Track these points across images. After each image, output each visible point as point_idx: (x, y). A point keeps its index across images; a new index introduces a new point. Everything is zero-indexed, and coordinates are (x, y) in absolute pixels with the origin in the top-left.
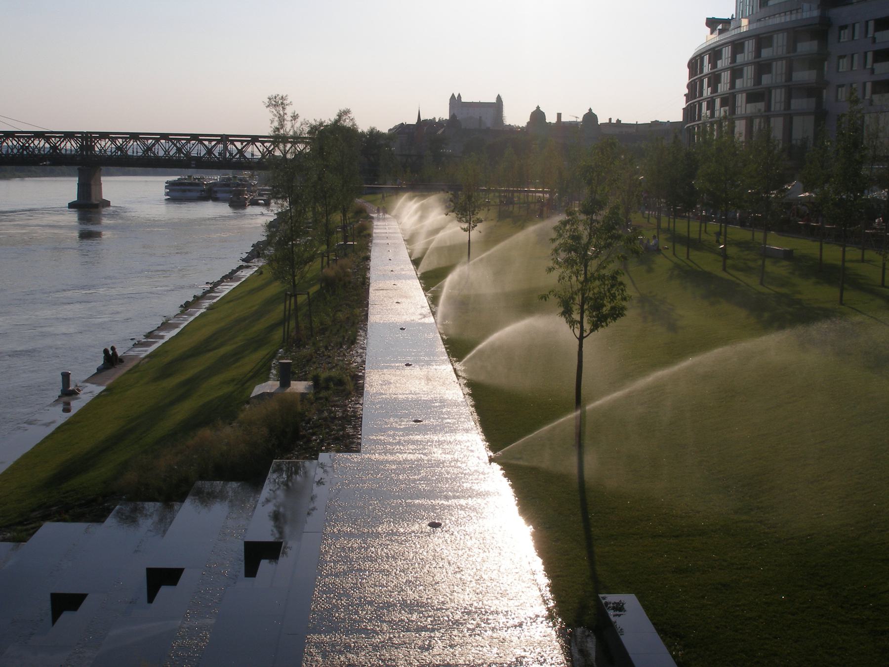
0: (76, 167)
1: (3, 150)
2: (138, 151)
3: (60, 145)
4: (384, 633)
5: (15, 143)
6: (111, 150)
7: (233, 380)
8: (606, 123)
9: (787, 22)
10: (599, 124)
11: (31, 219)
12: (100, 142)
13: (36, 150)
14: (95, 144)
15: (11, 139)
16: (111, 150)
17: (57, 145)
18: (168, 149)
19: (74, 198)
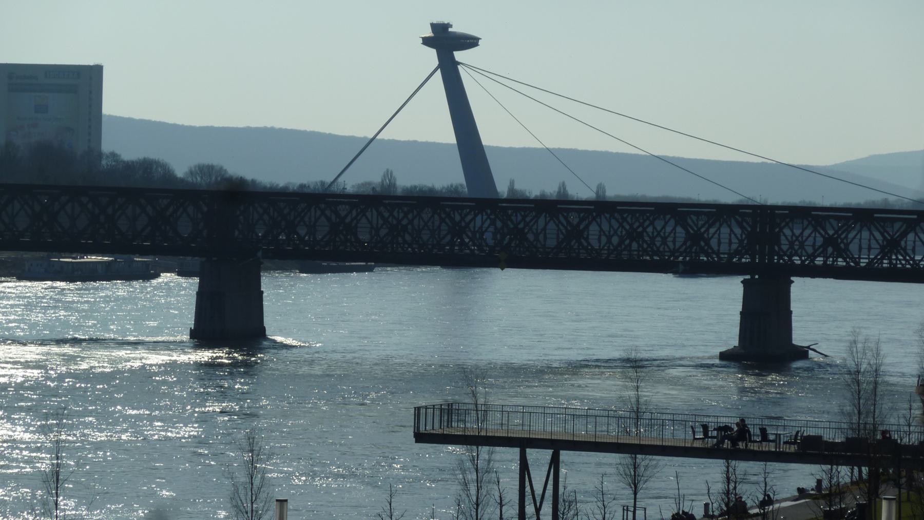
0: (741, 278)
1: (590, 237)
2: (873, 246)
3: (707, 230)
4: (41, 467)
5: (615, 224)
6: (814, 243)
7: (64, 355)
8: (201, 295)
9: (481, 445)
10: (914, 471)
11: (583, 336)
12: (790, 224)
13: (797, 243)
14: (781, 230)
15: (608, 216)
16: (814, 243)
17: (703, 230)
18: (481, 227)
19: (731, 338)
